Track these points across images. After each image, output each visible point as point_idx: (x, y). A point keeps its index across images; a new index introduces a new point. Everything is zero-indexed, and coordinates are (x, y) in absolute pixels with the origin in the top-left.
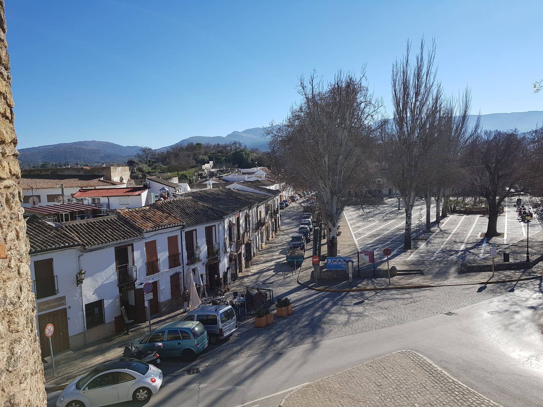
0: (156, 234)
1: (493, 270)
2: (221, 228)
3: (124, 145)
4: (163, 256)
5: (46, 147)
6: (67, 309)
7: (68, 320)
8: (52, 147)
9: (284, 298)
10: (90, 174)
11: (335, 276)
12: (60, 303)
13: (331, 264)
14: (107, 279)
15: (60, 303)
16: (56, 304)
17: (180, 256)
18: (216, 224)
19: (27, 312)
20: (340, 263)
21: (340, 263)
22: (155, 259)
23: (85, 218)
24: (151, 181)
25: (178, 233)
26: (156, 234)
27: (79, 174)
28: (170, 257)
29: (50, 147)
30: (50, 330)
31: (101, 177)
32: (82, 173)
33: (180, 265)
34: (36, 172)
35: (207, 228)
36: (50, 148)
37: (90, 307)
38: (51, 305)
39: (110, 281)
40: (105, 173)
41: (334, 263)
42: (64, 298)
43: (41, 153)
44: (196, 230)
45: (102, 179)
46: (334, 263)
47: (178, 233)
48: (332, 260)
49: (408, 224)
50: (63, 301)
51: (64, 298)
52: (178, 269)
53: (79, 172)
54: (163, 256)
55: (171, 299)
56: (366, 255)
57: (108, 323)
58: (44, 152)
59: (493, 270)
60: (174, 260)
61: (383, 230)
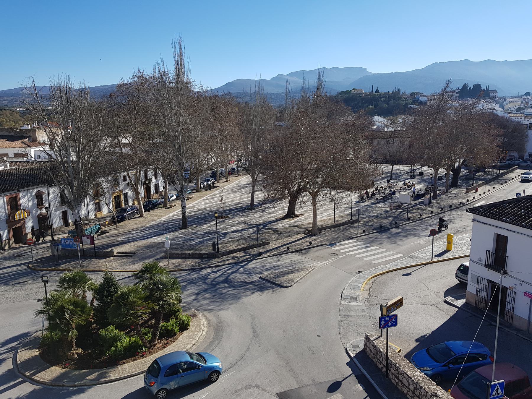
3: (404, 71)
5: (101, 88)
8: (107, 87)
9: (88, 276)
10: (19, 135)
11: (67, 254)
13: (65, 243)
20: (71, 243)
21: (71, 243)
23: (419, 174)
27: (10, 134)
40: (31, 135)
41: (67, 243)
43: (97, 93)
45: (26, 140)
46: (67, 243)
48: (65, 241)
49: (184, 212)
53: (10, 133)
56: (87, 238)
59: (168, 258)
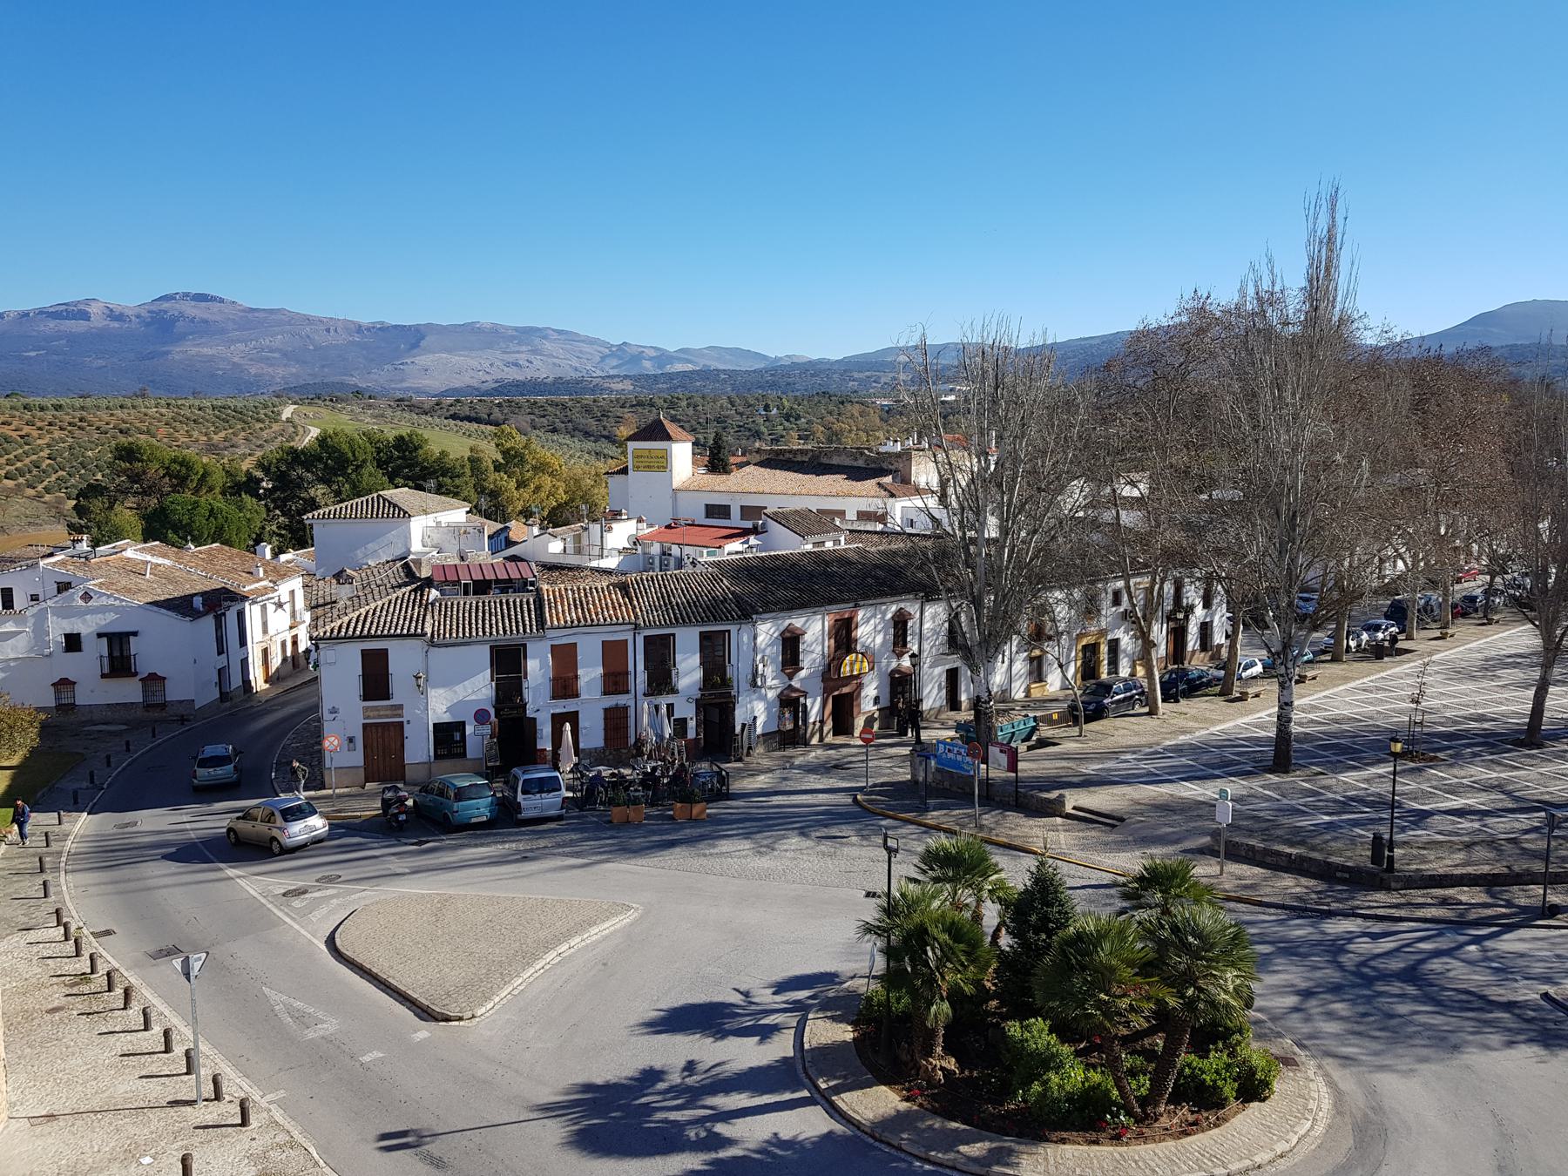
0: (574, 634)
1: (1222, 854)
2: (745, 638)
4: (590, 674)
6: (405, 723)
7: (406, 741)
10: (873, 466)
11: (947, 784)
12: (395, 713)
13: (944, 756)
14: (474, 692)
15: (395, 713)
16: (389, 712)
17: (631, 678)
18: (733, 628)
19: (1003, 759)
20: (959, 758)
22: (571, 675)
24: (769, 519)
25: (629, 636)
26: (574, 634)
27: (855, 464)
28: (606, 676)
29: (1093, 342)
30: (331, 743)
31: (884, 473)
32: (861, 463)
33: (627, 692)
34: (787, 455)
35: (704, 637)
36: (1091, 346)
37: (438, 727)
38: (382, 713)
39: (480, 697)
42: (400, 707)
44: (674, 635)
45: (888, 480)
46: (950, 755)
47: (629, 636)
50: (400, 712)
51: (400, 707)
52: (622, 700)
53: (856, 459)
54: (590, 674)
55: (604, 749)
56: (1001, 751)
57: (471, 759)
58: (1075, 356)
60: (615, 681)
61: (1445, 706)
